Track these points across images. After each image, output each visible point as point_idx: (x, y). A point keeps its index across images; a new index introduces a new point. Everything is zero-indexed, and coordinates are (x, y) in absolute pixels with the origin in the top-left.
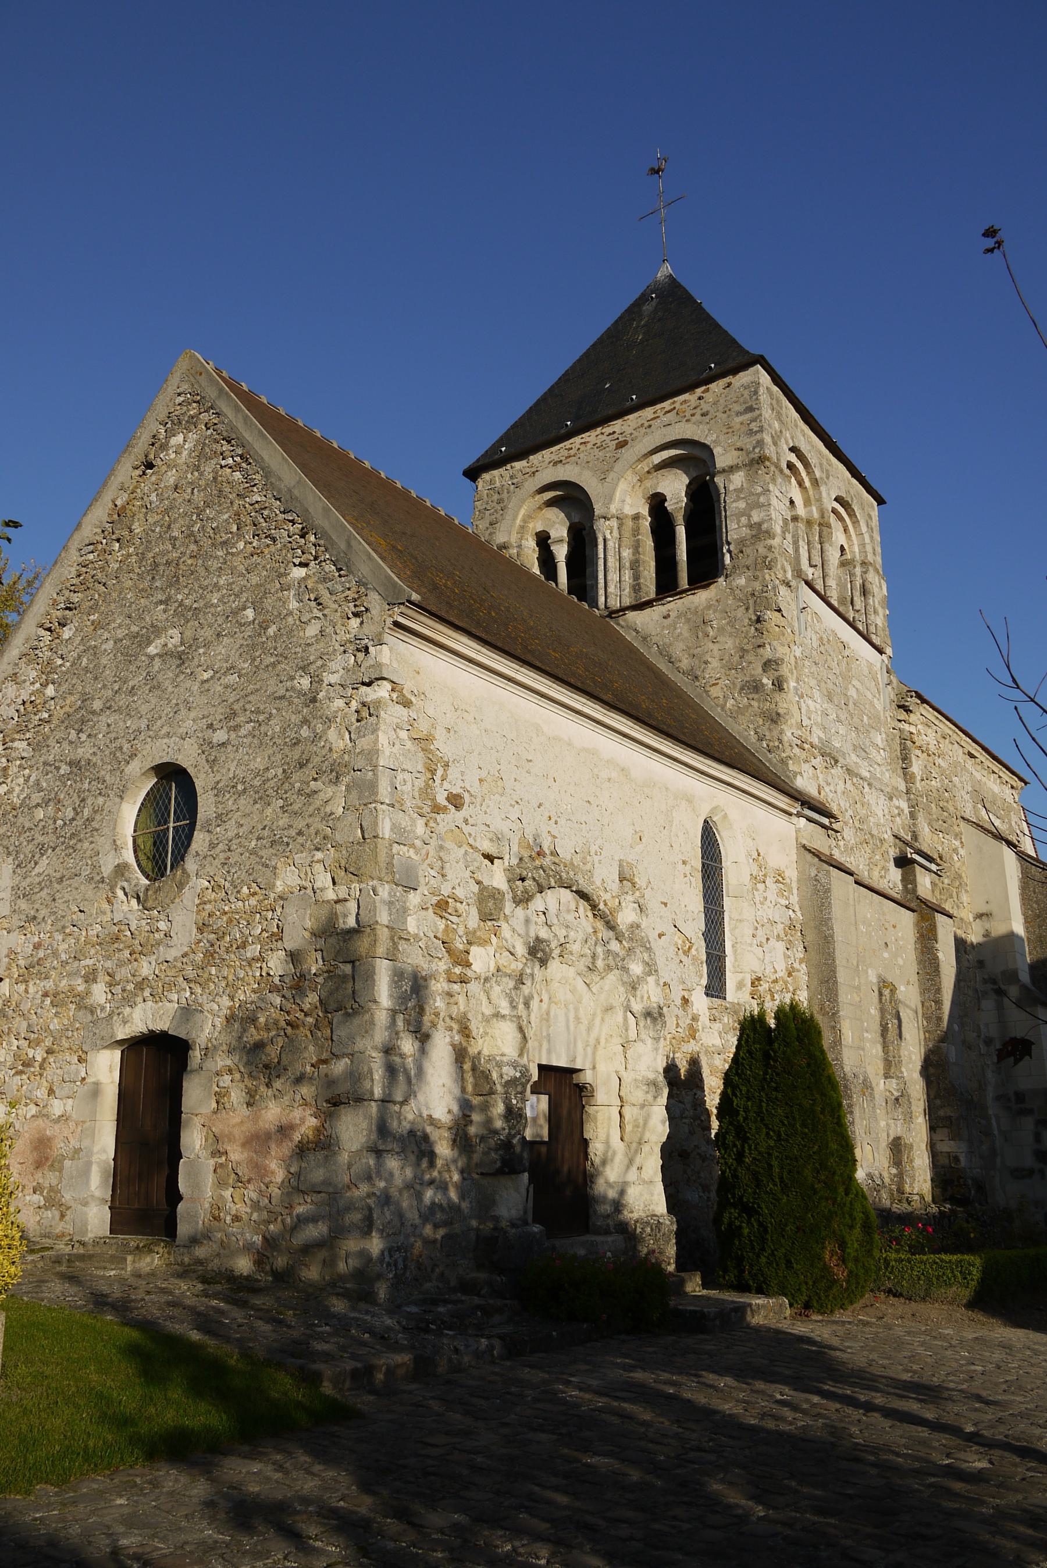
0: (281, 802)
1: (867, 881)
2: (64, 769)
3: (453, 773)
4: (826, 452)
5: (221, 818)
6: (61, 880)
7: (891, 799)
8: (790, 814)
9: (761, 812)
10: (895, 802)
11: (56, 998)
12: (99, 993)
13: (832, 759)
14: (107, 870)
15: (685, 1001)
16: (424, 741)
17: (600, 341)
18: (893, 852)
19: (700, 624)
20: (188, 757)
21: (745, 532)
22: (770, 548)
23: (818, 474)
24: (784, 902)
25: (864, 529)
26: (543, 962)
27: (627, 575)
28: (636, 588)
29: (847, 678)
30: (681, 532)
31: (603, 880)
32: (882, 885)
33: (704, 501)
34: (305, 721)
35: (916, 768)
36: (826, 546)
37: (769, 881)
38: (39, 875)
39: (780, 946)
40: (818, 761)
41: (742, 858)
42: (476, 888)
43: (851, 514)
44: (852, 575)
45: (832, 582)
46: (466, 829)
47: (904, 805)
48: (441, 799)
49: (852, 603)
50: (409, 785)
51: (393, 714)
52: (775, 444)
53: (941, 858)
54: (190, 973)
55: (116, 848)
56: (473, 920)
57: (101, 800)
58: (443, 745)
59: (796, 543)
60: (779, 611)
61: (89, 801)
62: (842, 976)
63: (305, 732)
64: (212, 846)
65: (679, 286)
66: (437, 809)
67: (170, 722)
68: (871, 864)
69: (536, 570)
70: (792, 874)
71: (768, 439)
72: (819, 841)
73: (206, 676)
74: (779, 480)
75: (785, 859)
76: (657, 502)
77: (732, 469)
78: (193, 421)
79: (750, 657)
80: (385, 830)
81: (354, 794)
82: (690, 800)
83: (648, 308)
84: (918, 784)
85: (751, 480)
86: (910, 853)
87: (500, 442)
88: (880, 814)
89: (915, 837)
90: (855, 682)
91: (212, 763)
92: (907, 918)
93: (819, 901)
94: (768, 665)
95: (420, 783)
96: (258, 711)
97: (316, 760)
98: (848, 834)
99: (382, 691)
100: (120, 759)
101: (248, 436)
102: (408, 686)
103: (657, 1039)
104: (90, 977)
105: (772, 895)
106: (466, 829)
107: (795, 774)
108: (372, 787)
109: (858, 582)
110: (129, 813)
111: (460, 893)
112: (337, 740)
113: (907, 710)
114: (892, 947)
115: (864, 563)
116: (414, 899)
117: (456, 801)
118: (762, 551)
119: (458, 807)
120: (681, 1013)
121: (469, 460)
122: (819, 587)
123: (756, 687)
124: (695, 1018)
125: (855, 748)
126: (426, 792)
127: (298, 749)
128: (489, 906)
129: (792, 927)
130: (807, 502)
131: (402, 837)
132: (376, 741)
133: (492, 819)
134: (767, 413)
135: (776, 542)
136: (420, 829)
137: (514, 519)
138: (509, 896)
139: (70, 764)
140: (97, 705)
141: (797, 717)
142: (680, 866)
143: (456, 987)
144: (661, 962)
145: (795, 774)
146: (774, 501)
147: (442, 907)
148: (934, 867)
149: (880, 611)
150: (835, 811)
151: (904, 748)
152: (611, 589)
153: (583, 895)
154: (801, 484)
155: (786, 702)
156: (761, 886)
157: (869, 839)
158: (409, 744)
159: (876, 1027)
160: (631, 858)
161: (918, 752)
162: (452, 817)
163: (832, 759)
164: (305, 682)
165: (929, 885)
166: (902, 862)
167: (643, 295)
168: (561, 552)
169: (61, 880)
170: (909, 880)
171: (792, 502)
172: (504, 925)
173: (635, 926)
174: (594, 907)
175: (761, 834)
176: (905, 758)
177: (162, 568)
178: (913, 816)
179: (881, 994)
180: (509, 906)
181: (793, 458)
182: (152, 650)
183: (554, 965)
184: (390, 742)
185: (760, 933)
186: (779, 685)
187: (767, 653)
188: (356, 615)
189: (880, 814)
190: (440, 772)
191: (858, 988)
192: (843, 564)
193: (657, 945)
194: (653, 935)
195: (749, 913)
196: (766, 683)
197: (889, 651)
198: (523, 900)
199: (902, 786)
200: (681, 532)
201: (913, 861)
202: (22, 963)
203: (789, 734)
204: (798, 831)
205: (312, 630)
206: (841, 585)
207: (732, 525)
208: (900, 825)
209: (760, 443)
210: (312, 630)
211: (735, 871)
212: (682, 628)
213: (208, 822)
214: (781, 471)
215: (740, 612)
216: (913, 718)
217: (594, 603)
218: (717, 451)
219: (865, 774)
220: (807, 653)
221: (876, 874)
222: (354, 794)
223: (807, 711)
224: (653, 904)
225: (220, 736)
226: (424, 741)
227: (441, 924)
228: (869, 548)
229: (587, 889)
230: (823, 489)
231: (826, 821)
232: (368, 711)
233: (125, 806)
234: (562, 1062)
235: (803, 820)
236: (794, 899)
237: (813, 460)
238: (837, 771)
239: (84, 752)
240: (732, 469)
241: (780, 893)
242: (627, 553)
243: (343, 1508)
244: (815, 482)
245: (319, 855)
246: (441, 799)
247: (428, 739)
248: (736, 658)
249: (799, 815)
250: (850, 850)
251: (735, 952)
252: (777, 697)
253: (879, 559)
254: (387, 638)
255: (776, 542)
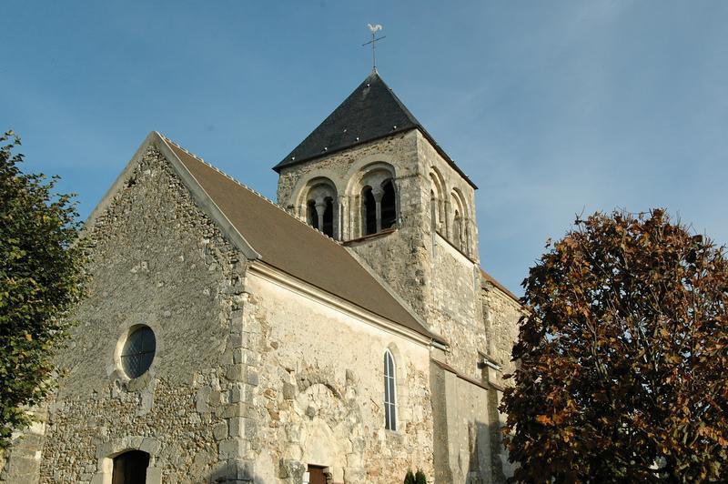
0: (196, 345)
1: (464, 375)
2: (87, 324)
3: (274, 333)
4: (449, 167)
5: (167, 351)
6: (85, 377)
7: (477, 334)
8: (426, 345)
9: (412, 345)
10: (480, 336)
11: (83, 433)
12: (104, 431)
13: (447, 315)
14: (109, 373)
15: (375, 434)
16: (261, 320)
17: (342, 106)
18: (477, 360)
19: (386, 252)
20: (151, 322)
21: (409, 208)
22: (420, 217)
23: (445, 178)
24: (423, 387)
25: (467, 202)
26: (311, 418)
27: (353, 224)
28: (357, 231)
29: (457, 277)
30: (378, 205)
31: (338, 379)
32: (472, 377)
33: (390, 191)
34: (208, 309)
35: (490, 318)
36: (449, 213)
37: (416, 377)
38: (73, 374)
39: (420, 408)
40: (441, 318)
41: (403, 366)
42: (282, 384)
43: (461, 196)
44: (461, 224)
45: (451, 230)
46: (279, 358)
47: (484, 337)
48: (269, 345)
49: (461, 238)
50: (255, 341)
51: (248, 308)
52: (424, 166)
53: (502, 362)
54: (151, 422)
55: (114, 363)
56: (281, 399)
57: (106, 340)
58: (270, 321)
59: (433, 211)
60: (424, 247)
61: (101, 340)
62: (449, 422)
63: (208, 314)
64: (163, 364)
65: (381, 81)
66: (267, 350)
67: (143, 304)
68: (466, 367)
69: (304, 219)
70: (427, 373)
71: (420, 164)
72: (440, 357)
73: (160, 285)
74: (425, 184)
75: (424, 367)
76: (367, 192)
77: (403, 178)
78: (156, 164)
79: (410, 268)
80: (245, 359)
81: (231, 343)
82: (379, 340)
83: (365, 92)
84: (491, 326)
85: (412, 183)
86: (486, 362)
87: (292, 154)
88: (472, 342)
89: (489, 353)
90: (461, 278)
91: (163, 325)
92: (484, 393)
93: (439, 385)
94: (417, 273)
95: (259, 338)
96: (186, 303)
97: (214, 327)
98: (455, 352)
99: (244, 298)
100: (116, 321)
101: (182, 173)
102: (255, 294)
103: (361, 453)
104: (101, 423)
105: (417, 384)
106: (279, 358)
107: (430, 325)
108: (239, 341)
109: (464, 227)
110: (121, 347)
111: (275, 387)
112: (222, 318)
113: (487, 290)
114: (476, 407)
115: (466, 219)
116: (256, 390)
117: (275, 345)
118: (417, 218)
119: (276, 348)
120: (373, 440)
121: (276, 163)
122: (444, 235)
123: (413, 283)
124: (379, 443)
125: (460, 310)
126: (262, 342)
127: (205, 321)
128: (288, 394)
129: (426, 398)
130: (439, 191)
131: (252, 362)
132: (241, 320)
133: (290, 355)
134: (420, 152)
135: (423, 214)
136: (259, 359)
137: (298, 193)
138: (297, 388)
139: (91, 321)
140: (105, 294)
141: (431, 297)
142: (374, 371)
143: (274, 429)
144: (364, 416)
145: (430, 325)
146: (423, 194)
147: (267, 393)
148: (498, 368)
149: (474, 242)
150: (449, 342)
151: (484, 308)
152: (345, 231)
153: (329, 386)
154: (436, 183)
155: (427, 290)
156: (412, 380)
157: (465, 354)
158: (255, 321)
159: (467, 446)
160: (351, 368)
161: (492, 311)
162: (274, 352)
163: (447, 315)
164: (207, 292)
165: (495, 376)
166: (482, 366)
167: (363, 84)
168: (320, 211)
169: (85, 377)
170: (485, 374)
171: (432, 192)
172: (295, 402)
173: (352, 401)
174: (334, 392)
175: (414, 355)
176: (485, 314)
177: (139, 233)
178: (488, 342)
179: (469, 430)
180: (297, 393)
181: (432, 171)
182: (133, 270)
183: (316, 419)
184: (248, 320)
185: (411, 402)
186: (423, 283)
187: (417, 266)
188: (232, 262)
189: (472, 342)
190: (268, 333)
191: (457, 428)
192: (456, 219)
193: (363, 409)
194: (361, 404)
195: (406, 392)
196: (415, 283)
197: (478, 261)
198: (303, 389)
199: (483, 328)
200: (378, 205)
201: (488, 365)
202: (64, 416)
203: (427, 306)
204: (430, 352)
205: (212, 268)
206: (455, 230)
207: (403, 205)
208: (482, 348)
209: (417, 167)
210: (212, 268)
211: (401, 373)
212: (378, 253)
213: (161, 352)
214: (426, 179)
215: (406, 247)
216: (489, 294)
217: (336, 239)
218: (397, 168)
219: (465, 323)
220: (437, 266)
221: (469, 372)
222: (231, 343)
223: (436, 293)
224: (362, 390)
225: (167, 313)
226: (261, 320)
227: (267, 401)
228: (469, 211)
229: (331, 384)
230: (447, 185)
231: (444, 347)
232: (237, 308)
233: (119, 343)
234: (319, 463)
235: (433, 348)
236: (428, 385)
237: (442, 171)
238: (450, 323)
239: (98, 316)
240: (403, 178)
241: (421, 383)
242: (352, 214)
243: (431, 384)
244: (443, 182)
245: (214, 370)
246: (269, 345)
247: (264, 318)
248: (403, 268)
249: (431, 345)
250: (455, 360)
251: (399, 410)
252: (422, 288)
253: (474, 216)
254: (247, 274)
255: (423, 214)
